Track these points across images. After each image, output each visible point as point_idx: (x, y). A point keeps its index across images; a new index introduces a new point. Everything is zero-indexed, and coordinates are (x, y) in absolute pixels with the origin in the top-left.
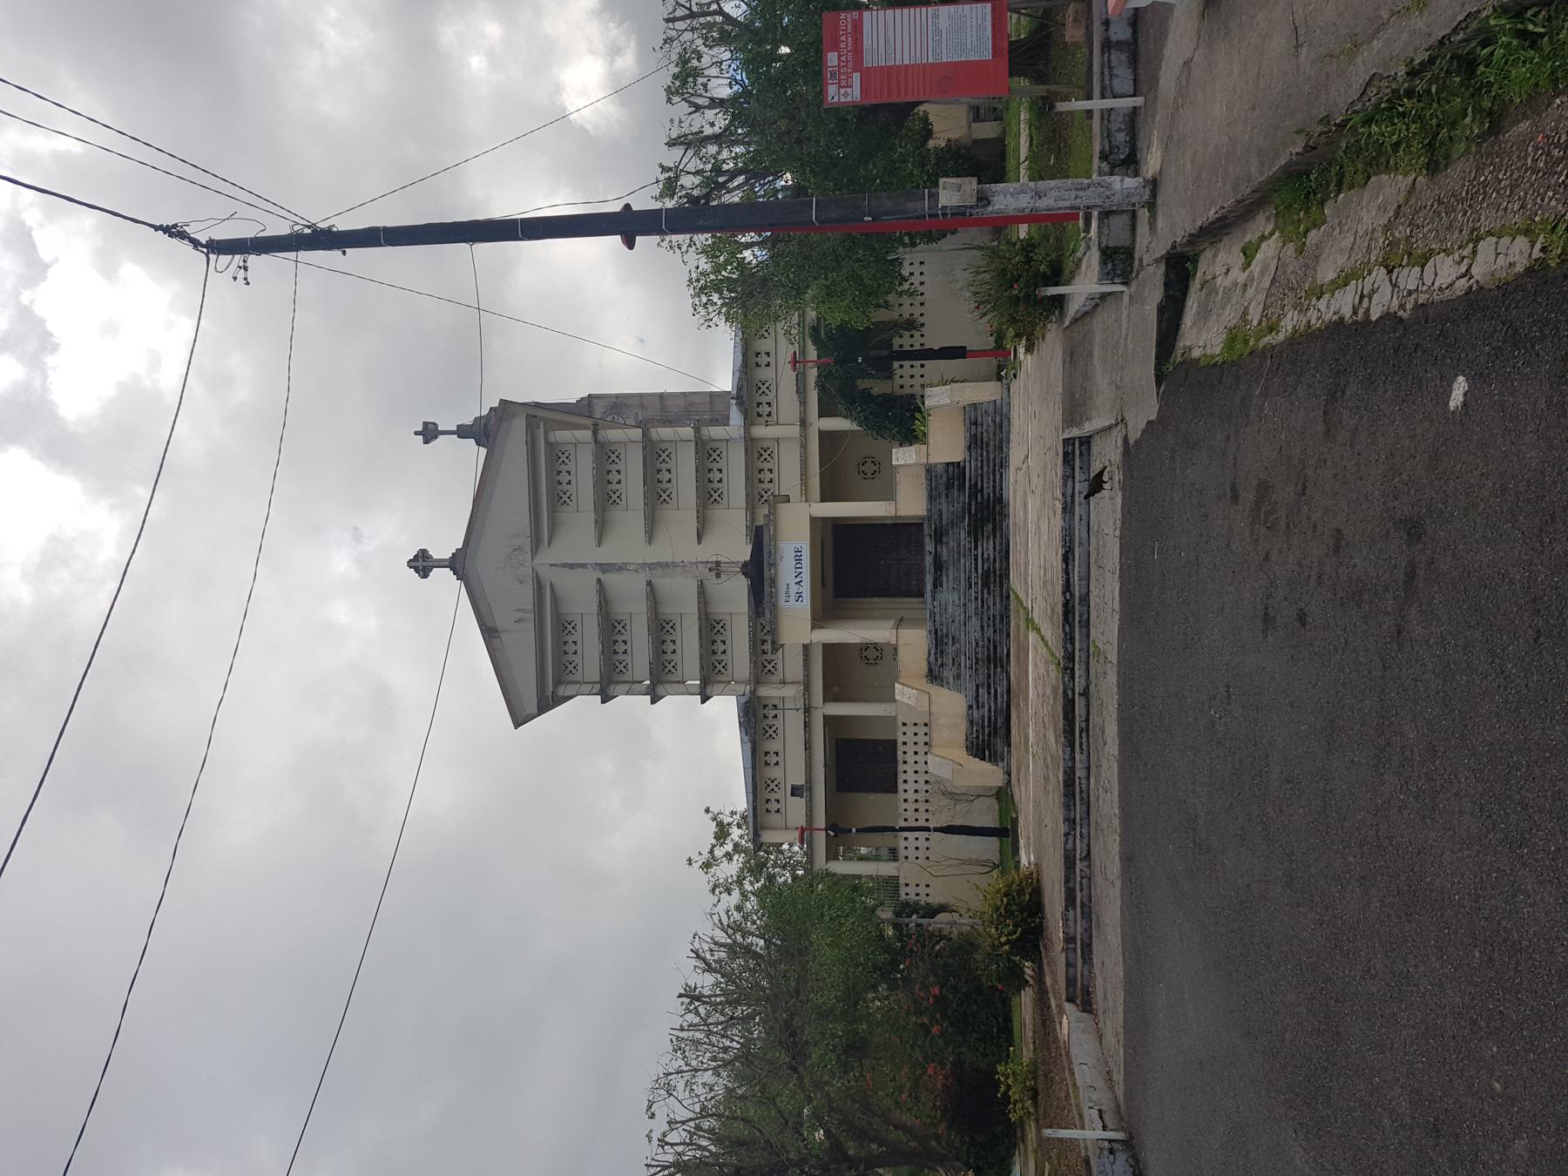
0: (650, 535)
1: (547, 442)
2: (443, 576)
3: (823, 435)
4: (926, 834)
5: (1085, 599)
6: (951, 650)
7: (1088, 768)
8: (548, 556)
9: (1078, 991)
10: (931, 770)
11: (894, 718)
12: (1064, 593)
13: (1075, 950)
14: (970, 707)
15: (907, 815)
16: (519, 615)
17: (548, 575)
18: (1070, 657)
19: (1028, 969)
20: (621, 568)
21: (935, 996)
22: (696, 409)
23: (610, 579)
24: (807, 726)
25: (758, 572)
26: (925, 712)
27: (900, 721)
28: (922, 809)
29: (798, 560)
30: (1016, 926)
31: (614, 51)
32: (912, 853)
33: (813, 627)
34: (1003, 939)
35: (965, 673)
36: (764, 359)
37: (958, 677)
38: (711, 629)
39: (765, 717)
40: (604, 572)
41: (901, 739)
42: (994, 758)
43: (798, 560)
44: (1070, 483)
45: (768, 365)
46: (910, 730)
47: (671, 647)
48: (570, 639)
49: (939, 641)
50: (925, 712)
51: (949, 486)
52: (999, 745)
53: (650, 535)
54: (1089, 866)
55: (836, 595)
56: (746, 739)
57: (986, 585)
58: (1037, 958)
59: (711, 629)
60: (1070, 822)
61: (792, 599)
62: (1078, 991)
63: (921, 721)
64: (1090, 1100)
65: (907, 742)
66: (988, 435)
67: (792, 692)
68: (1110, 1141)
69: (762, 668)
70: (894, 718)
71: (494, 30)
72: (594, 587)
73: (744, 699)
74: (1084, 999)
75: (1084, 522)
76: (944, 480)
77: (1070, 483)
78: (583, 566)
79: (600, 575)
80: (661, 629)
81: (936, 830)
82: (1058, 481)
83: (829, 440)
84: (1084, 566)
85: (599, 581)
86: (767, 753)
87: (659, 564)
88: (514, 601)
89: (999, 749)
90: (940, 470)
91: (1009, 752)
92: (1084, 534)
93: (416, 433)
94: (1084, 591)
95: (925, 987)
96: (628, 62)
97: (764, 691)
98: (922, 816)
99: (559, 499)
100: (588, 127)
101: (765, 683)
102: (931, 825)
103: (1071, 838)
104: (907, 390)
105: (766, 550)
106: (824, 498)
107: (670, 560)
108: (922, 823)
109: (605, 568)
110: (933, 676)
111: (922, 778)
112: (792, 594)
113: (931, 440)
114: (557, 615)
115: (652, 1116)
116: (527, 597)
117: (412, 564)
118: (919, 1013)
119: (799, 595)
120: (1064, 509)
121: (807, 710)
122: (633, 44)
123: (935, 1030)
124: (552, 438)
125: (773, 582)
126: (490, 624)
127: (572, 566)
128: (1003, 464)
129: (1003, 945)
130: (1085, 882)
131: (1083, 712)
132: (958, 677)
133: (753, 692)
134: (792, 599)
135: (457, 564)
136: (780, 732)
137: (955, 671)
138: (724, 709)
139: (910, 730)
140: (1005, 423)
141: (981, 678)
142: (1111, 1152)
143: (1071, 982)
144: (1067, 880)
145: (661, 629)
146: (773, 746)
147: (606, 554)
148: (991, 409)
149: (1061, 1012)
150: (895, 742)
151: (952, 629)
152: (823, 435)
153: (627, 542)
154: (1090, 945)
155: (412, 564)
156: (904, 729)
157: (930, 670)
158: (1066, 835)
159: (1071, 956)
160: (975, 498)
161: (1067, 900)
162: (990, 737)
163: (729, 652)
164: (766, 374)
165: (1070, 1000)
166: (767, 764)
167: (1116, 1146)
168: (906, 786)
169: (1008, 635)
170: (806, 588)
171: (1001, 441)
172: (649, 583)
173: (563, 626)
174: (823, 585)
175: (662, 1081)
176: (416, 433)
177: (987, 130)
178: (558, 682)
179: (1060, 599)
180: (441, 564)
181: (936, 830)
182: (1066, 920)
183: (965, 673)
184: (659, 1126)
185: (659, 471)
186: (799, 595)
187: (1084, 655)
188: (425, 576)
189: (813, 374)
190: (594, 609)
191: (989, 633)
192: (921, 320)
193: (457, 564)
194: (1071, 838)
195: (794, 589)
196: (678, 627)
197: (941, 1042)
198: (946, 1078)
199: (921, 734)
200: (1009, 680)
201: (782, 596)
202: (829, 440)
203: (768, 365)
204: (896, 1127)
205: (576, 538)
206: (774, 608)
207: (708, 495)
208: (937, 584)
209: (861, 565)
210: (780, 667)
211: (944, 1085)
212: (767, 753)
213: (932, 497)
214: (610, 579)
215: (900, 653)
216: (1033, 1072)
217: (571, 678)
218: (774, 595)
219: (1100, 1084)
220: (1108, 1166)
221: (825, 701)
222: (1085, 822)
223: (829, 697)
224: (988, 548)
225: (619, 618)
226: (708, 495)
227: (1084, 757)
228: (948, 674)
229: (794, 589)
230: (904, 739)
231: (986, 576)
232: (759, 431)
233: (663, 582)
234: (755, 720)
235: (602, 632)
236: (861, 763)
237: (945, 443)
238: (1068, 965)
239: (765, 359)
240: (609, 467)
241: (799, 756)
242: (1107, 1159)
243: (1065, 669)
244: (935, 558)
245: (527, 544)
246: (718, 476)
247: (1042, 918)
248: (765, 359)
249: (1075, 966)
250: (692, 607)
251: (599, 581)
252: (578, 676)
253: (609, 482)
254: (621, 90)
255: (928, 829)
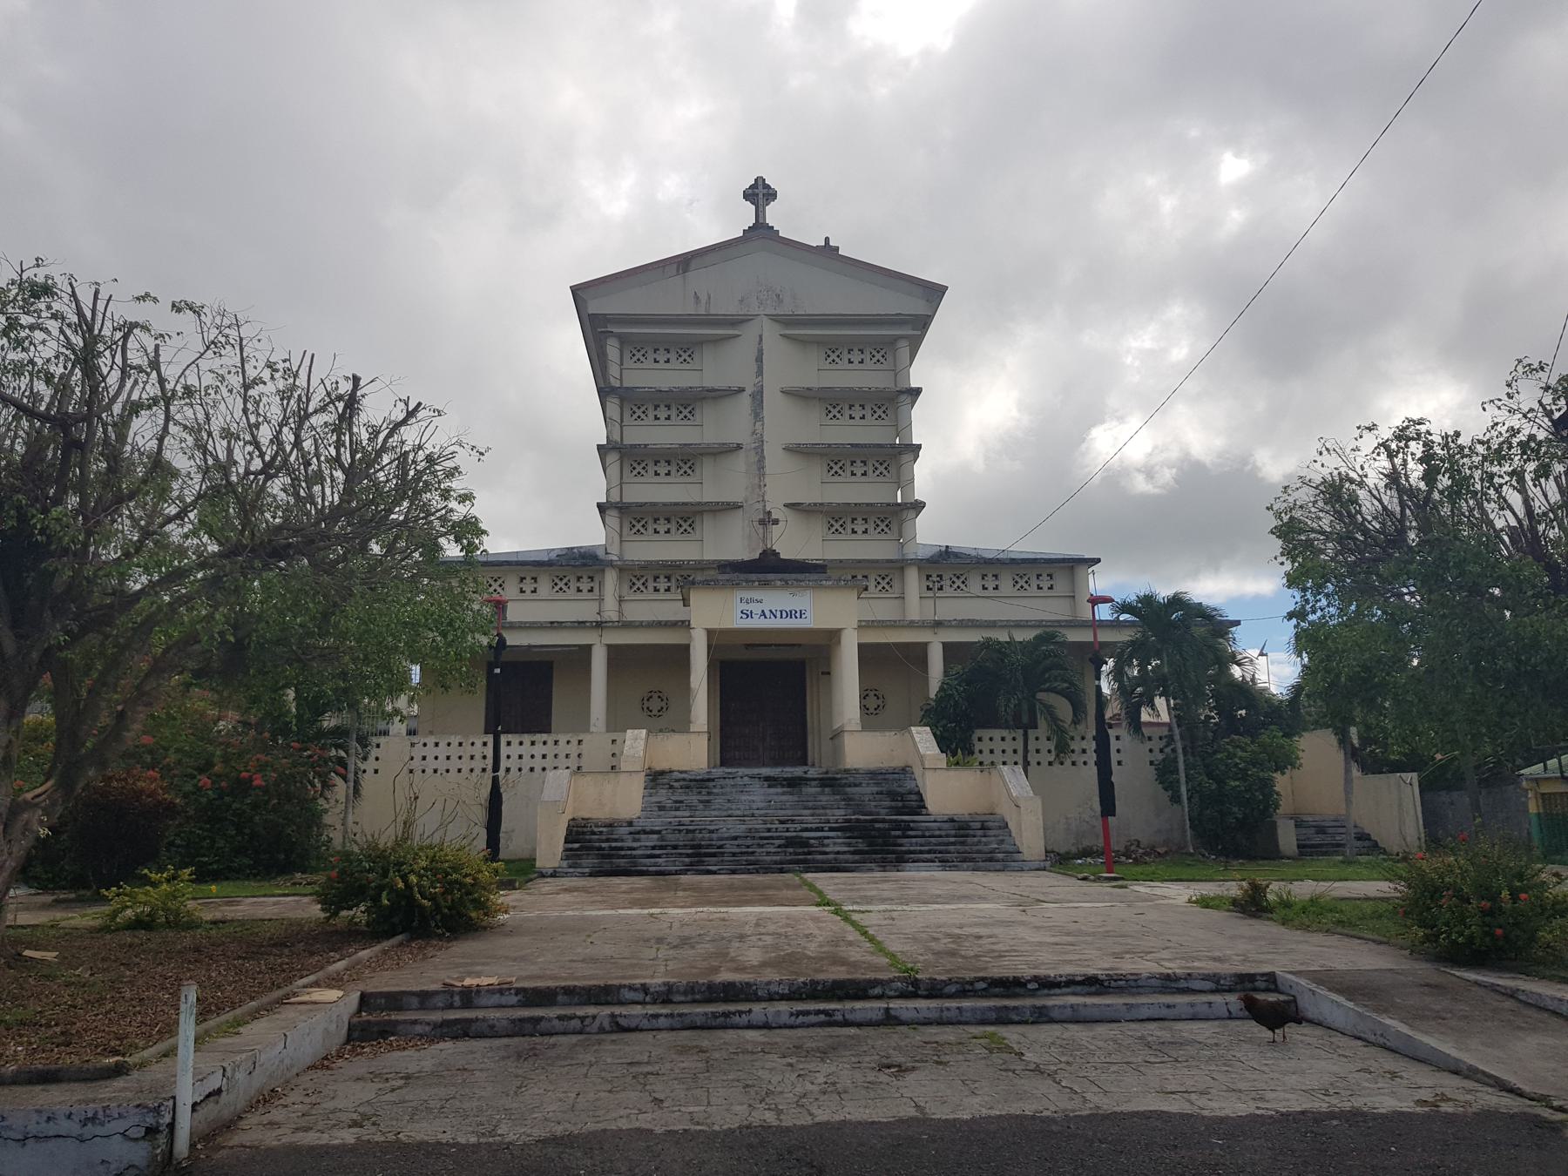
0: (796, 450)
1: (902, 337)
2: (746, 215)
3: (923, 647)
4: (490, 767)
5: (1042, 1017)
6: (693, 798)
7: (766, 1026)
8: (771, 333)
9: (384, 1016)
10: (550, 774)
11: (587, 730)
12: (1036, 979)
13: (451, 1007)
14: (630, 824)
15: (467, 745)
16: (704, 298)
17: (749, 334)
18: (934, 990)
19: (358, 913)
20: (757, 415)
21: (251, 779)
22: (898, 514)
23: (745, 401)
24: (581, 625)
25: (768, 568)
26: (600, 768)
27: (585, 737)
28: (473, 764)
29: (790, 614)
30: (433, 898)
31: (1149, 472)
32: (418, 751)
33: (710, 633)
34: (413, 879)
35: (670, 818)
36: (991, 584)
37: (662, 808)
38: (685, 517)
39: (579, 579)
40: (753, 396)
41: (550, 738)
42: (569, 854)
43: (790, 614)
44: (1209, 985)
45: (522, 591)
46: (573, 749)
47: (663, 470)
48: (672, 356)
49: (700, 784)
50: (600, 768)
51: (892, 795)
52: (589, 862)
53: (796, 450)
54: (602, 1030)
55: (722, 662)
56: (553, 556)
57: (790, 842)
58: (376, 932)
59: (685, 517)
60: (665, 996)
61: (745, 607)
62: (384, 1016)
63: (584, 762)
64: (236, 1067)
65: (559, 742)
66: (974, 844)
67: (611, 611)
68: (172, 1126)
69: (639, 575)
70: (587, 730)
71: (1180, 353)
72: (735, 384)
73: (601, 554)
74: (373, 1026)
75: (1164, 1012)
76: (900, 794)
77: (1209, 985)
78: (760, 372)
79: (749, 391)
80: (685, 460)
81: (495, 781)
82: (1206, 966)
83: (918, 654)
84: (1096, 1014)
85: (742, 390)
86: (535, 579)
87: (762, 459)
88: (720, 294)
89: (584, 862)
90: (909, 785)
91: (583, 875)
92: (1145, 1013)
93: (827, 239)
94: (1055, 1014)
95: (262, 768)
96: (1141, 485)
97: (611, 578)
98: (513, 764)
99: (832, 349)
100: (1084, 446)
101: (620, 578)
102: (501, 773)
103: (640, 996)
104: (978, 746)
105: (799, 576)
106: (863, 648)
107: (767, 470)
108: (504, 764)
109: (758, 397)
110: (656, 778)
111: (538, 763)
112: (751, 607)
113: (952, 773)
114: (701, 342)
115: (176, 308)
116: (725, 306)
117: (760, 183)
118: (226, 760)
119: (749, 615)
120: (1167, 977)
121: (599, 625)
122: (1157, 491)
123: (204, 780)
124: (903, 343)
125: (765, 584)
126: (693, 265)
127: (759, 359)
128: (946, 864)
129: (404, 878)
130: (576, 1023)
131: (858, 1017)
132: (662, 808)
133: (611, 564)
134: (745, 607)
135: (760, 231)
136: (561, 595)
137: (669, 804)
138: (588, 531)
139: (573, 749)
140: (998, 865)
141: (672, 838)
142: (151, 1131)
143: (395, 1001)
144: (569, 991)
145: (685, 460)
146: (544, 588)
147: (774, 402)
148: (1011, 848)
149: (335, 982)
150: (548, 731)
151: (720, 800)
152: (923, 647)
153: (786, 424)
154: (466, 1035)
155: (760, 183)
156: (574, 742)
157: (662, 773)
158: (645, 989)
159: (439, 1001)
160: (888, 831)
161: (537, 992)
162: (596, 850)
163: (854, 536)
164: (975, 585)
165: (365, 1000)
166: (522, 579)
167: (162, 1139)
168: (442, 745)
169: (734, 872)
170: (757, 623)
171: (972, 860)
172: (739, 447)
173: (687, 349)
174: (748, 646)
175: (233, 333)
176: (827, 239)
177: (1287, 838)
178: (623, 340)
179: (1026, 972)
180: (760, 213)
181: (495, 781)
182: (501, 990)
183: (670, 818)
184: (159, 317)
185: (864, 463)
186: (749, 615)
187: (953, 1014)
188: (746, 196)
189: (1003, 637)
190: (708, 384)
191: (730, 847)
192: (1068, 762)
193: (760, 231)
194: (640, 996)
195: (756, 609)
196: (686, 479)
197: (188, 787)
198: (152, 794)
199: (435, 765)
200: (677, 873)
201: (747, 594)
202: (918, 654)
203: (1039, 588)
204: (121, 716)
205: (789, 367)
206: (736, 585)
207: (838, 517)
208: (771, 781)
209: (767, 693)
210: (639, 596)
211: (142, 791)
212: (535, 579)
213: (875, 775)
214: (745, 401)
215: (677, 737)
216: (181, 923)
217: (627, 355)
218: (749, 585)
219: (259, 1080)
220: (120, 1126)
221: (609, 646)
222: (676, 1022)
223: (615, 653)
224: (836, 845)
225: (697, 412)
226: (838, 517)
227: (785, 1019)
228: (663, 795)
229: (756, 609)
230: (562, 742)
231: (804, 843)
232: (913, 579)
233: (740, 463)
234: (576, 566)
235: (683, 391)
236: (522, 691)
237: (947, 790)
238: (424, 998)
239: (991, 585)
240: (868, 408)
241: (534, 618)
242: (134, 1122)
243: (916, 983)
244: (801, 779)
245: (786, 309)
246: (860, 529)
247: (440, 937)
248: (991, 585)
249: (423, 1007)
250: (709, 495)
251: (742, 390)
252: (628, 363)
253: (851, 407)
254: (1115, 477)
255: (496, 768)
